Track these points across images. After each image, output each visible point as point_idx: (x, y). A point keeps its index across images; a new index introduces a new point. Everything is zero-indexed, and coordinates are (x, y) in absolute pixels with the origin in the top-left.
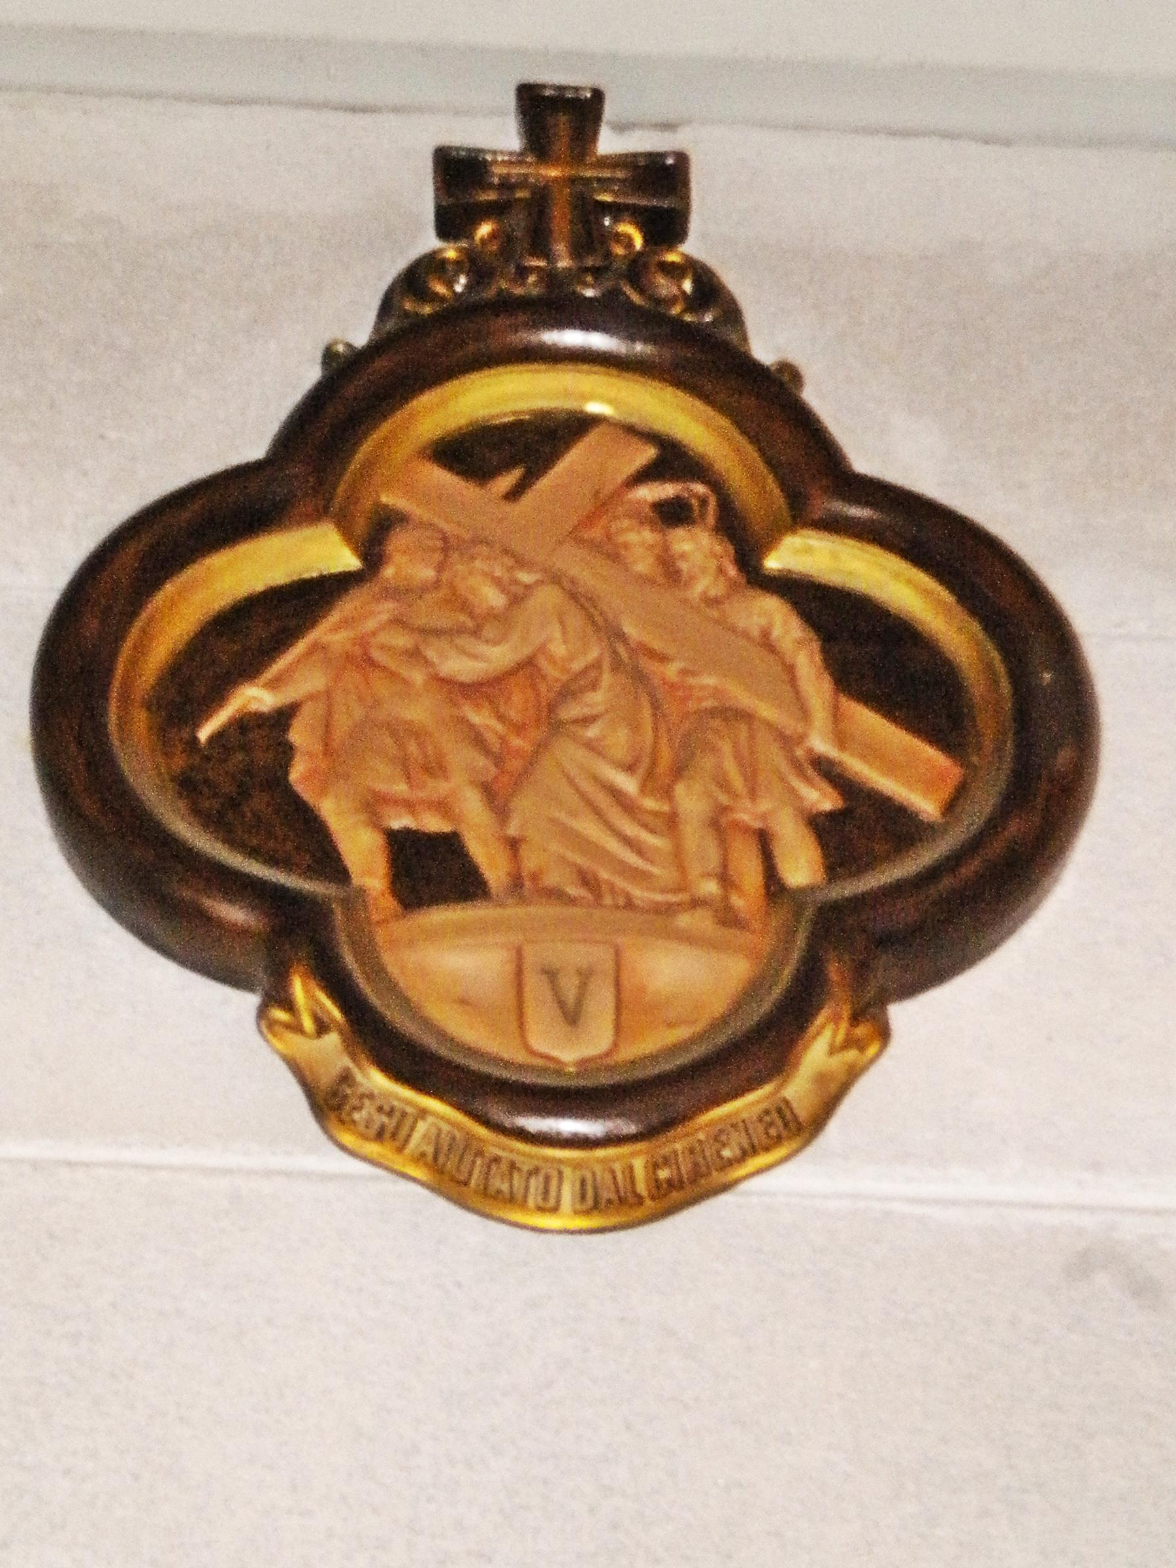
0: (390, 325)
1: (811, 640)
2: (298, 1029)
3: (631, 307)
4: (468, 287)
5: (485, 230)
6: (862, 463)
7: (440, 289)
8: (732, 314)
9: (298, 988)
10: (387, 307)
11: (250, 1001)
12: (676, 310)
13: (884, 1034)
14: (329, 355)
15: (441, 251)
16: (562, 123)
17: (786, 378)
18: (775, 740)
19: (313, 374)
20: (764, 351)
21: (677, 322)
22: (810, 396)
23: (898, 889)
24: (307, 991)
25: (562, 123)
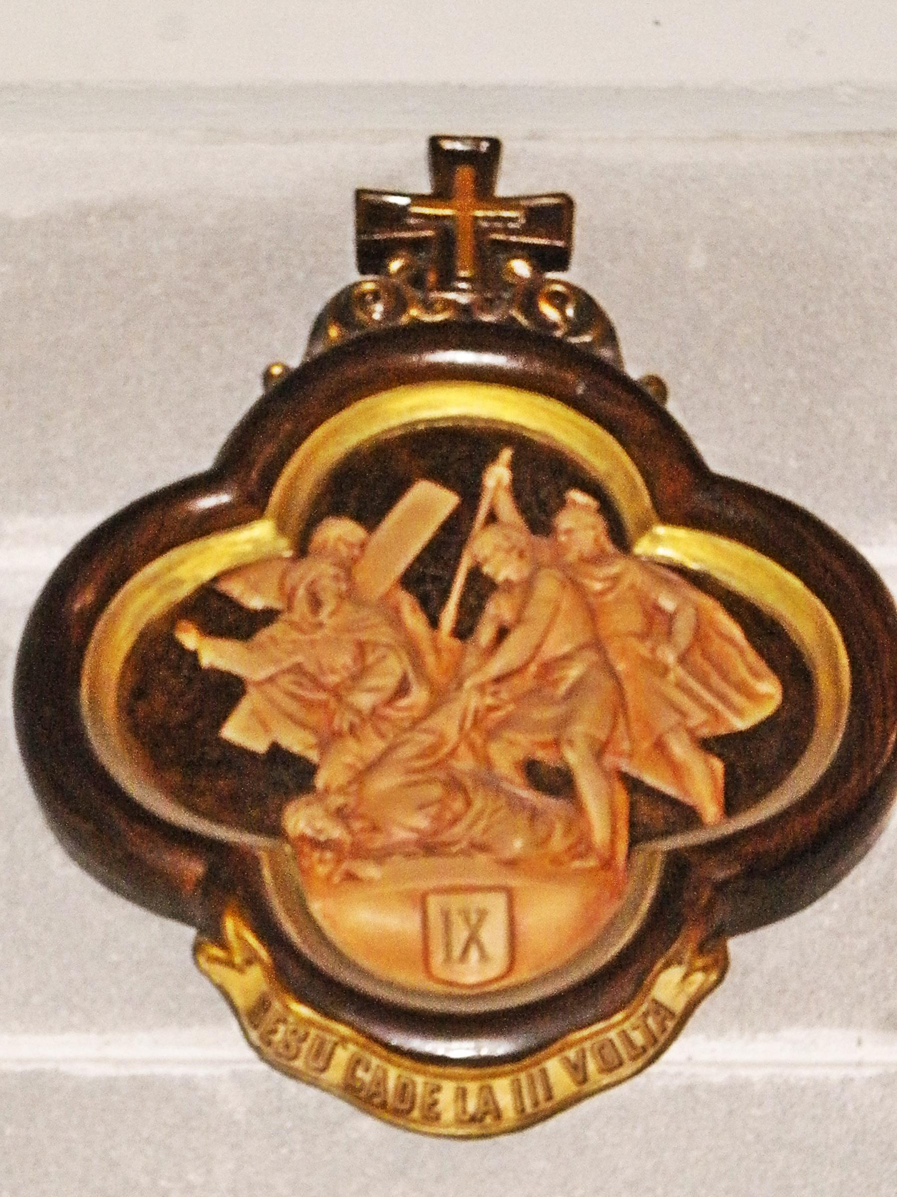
0: (319, 349)
1: (244, 742)
2: (229, 963)
3: (522, 330)
4: (387, 314)
5: (395, 265)
6: (716, 465)
8: (609, 336)
9: (231, 925)
10: (318, 329)
11: (190, 933)
12: (558, 334)
13: (722, 965)
14: (267, 376)
15: (357, 285)
16: (464, 174)
17: (650, 390)
18: (190, 860)
19: (257, 392)
20: (634, 371)
21: (560, 342)
22: (672, 407)
23: (783, 816)
24: (236, 926)
25: (464, 174)
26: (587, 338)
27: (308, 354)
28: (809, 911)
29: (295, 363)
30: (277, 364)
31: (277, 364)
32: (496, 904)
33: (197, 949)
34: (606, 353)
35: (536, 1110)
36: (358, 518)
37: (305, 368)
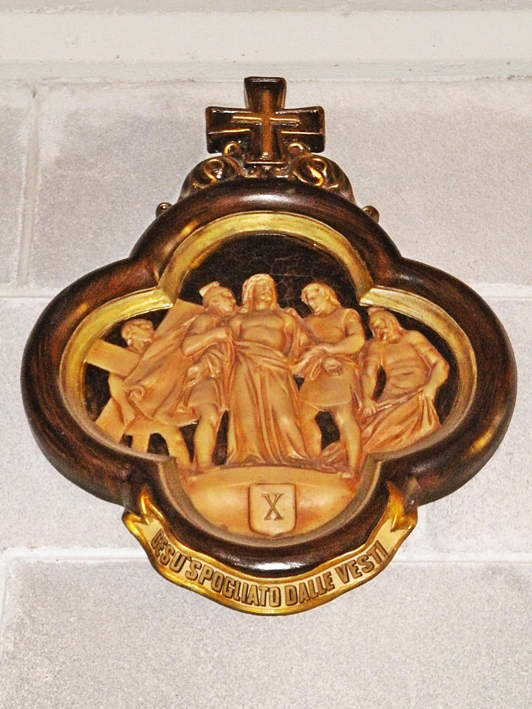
0: (187, 195)
6: (405, 254)
7: (211, 177)
8: (346, 184)
10: (186, 185)
14: (160, 209)
16: (266, 97)
19: (153, 218)
20: (361, 204)
22: (382, 223)
26: (336, 186)
27: (180, 198)
28: (43, 458)
29: (174, 201)
30: (163, 203)
31: (163, 203)
32: (288, 493)
33: (125, 517)
34: (345, 195)
35: (130, 511)
36: (107, 378)
37: (177, 206)
